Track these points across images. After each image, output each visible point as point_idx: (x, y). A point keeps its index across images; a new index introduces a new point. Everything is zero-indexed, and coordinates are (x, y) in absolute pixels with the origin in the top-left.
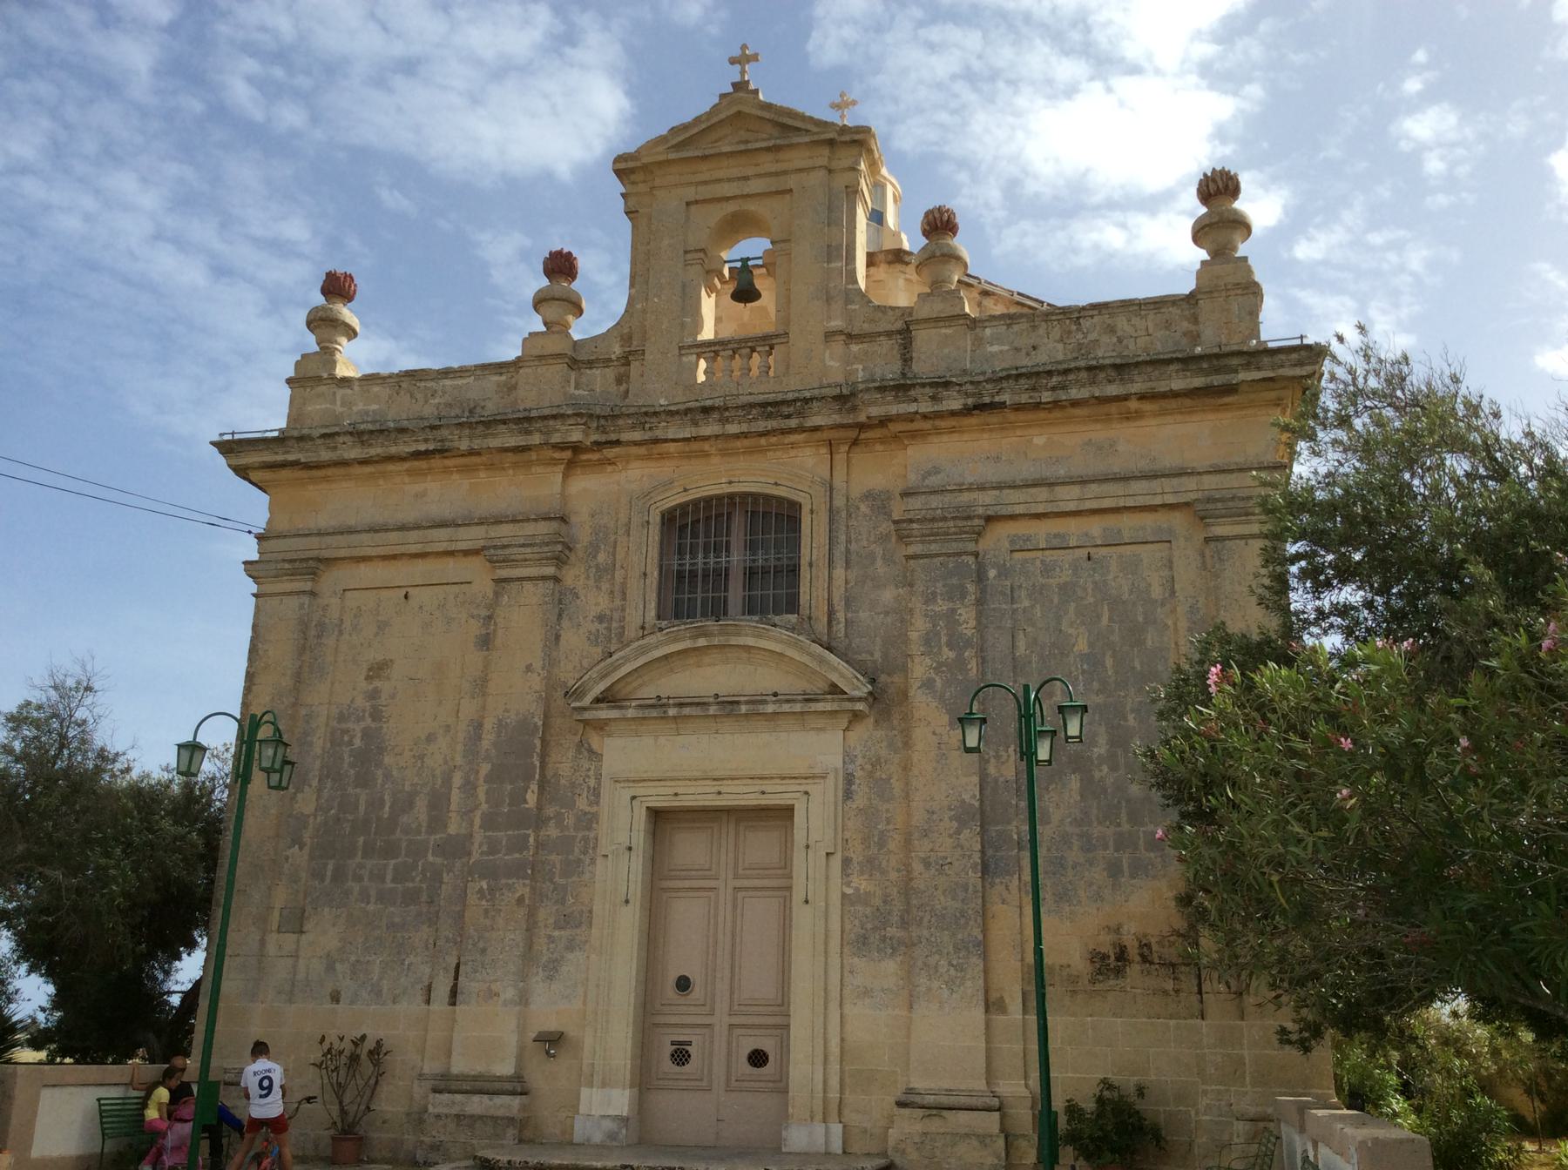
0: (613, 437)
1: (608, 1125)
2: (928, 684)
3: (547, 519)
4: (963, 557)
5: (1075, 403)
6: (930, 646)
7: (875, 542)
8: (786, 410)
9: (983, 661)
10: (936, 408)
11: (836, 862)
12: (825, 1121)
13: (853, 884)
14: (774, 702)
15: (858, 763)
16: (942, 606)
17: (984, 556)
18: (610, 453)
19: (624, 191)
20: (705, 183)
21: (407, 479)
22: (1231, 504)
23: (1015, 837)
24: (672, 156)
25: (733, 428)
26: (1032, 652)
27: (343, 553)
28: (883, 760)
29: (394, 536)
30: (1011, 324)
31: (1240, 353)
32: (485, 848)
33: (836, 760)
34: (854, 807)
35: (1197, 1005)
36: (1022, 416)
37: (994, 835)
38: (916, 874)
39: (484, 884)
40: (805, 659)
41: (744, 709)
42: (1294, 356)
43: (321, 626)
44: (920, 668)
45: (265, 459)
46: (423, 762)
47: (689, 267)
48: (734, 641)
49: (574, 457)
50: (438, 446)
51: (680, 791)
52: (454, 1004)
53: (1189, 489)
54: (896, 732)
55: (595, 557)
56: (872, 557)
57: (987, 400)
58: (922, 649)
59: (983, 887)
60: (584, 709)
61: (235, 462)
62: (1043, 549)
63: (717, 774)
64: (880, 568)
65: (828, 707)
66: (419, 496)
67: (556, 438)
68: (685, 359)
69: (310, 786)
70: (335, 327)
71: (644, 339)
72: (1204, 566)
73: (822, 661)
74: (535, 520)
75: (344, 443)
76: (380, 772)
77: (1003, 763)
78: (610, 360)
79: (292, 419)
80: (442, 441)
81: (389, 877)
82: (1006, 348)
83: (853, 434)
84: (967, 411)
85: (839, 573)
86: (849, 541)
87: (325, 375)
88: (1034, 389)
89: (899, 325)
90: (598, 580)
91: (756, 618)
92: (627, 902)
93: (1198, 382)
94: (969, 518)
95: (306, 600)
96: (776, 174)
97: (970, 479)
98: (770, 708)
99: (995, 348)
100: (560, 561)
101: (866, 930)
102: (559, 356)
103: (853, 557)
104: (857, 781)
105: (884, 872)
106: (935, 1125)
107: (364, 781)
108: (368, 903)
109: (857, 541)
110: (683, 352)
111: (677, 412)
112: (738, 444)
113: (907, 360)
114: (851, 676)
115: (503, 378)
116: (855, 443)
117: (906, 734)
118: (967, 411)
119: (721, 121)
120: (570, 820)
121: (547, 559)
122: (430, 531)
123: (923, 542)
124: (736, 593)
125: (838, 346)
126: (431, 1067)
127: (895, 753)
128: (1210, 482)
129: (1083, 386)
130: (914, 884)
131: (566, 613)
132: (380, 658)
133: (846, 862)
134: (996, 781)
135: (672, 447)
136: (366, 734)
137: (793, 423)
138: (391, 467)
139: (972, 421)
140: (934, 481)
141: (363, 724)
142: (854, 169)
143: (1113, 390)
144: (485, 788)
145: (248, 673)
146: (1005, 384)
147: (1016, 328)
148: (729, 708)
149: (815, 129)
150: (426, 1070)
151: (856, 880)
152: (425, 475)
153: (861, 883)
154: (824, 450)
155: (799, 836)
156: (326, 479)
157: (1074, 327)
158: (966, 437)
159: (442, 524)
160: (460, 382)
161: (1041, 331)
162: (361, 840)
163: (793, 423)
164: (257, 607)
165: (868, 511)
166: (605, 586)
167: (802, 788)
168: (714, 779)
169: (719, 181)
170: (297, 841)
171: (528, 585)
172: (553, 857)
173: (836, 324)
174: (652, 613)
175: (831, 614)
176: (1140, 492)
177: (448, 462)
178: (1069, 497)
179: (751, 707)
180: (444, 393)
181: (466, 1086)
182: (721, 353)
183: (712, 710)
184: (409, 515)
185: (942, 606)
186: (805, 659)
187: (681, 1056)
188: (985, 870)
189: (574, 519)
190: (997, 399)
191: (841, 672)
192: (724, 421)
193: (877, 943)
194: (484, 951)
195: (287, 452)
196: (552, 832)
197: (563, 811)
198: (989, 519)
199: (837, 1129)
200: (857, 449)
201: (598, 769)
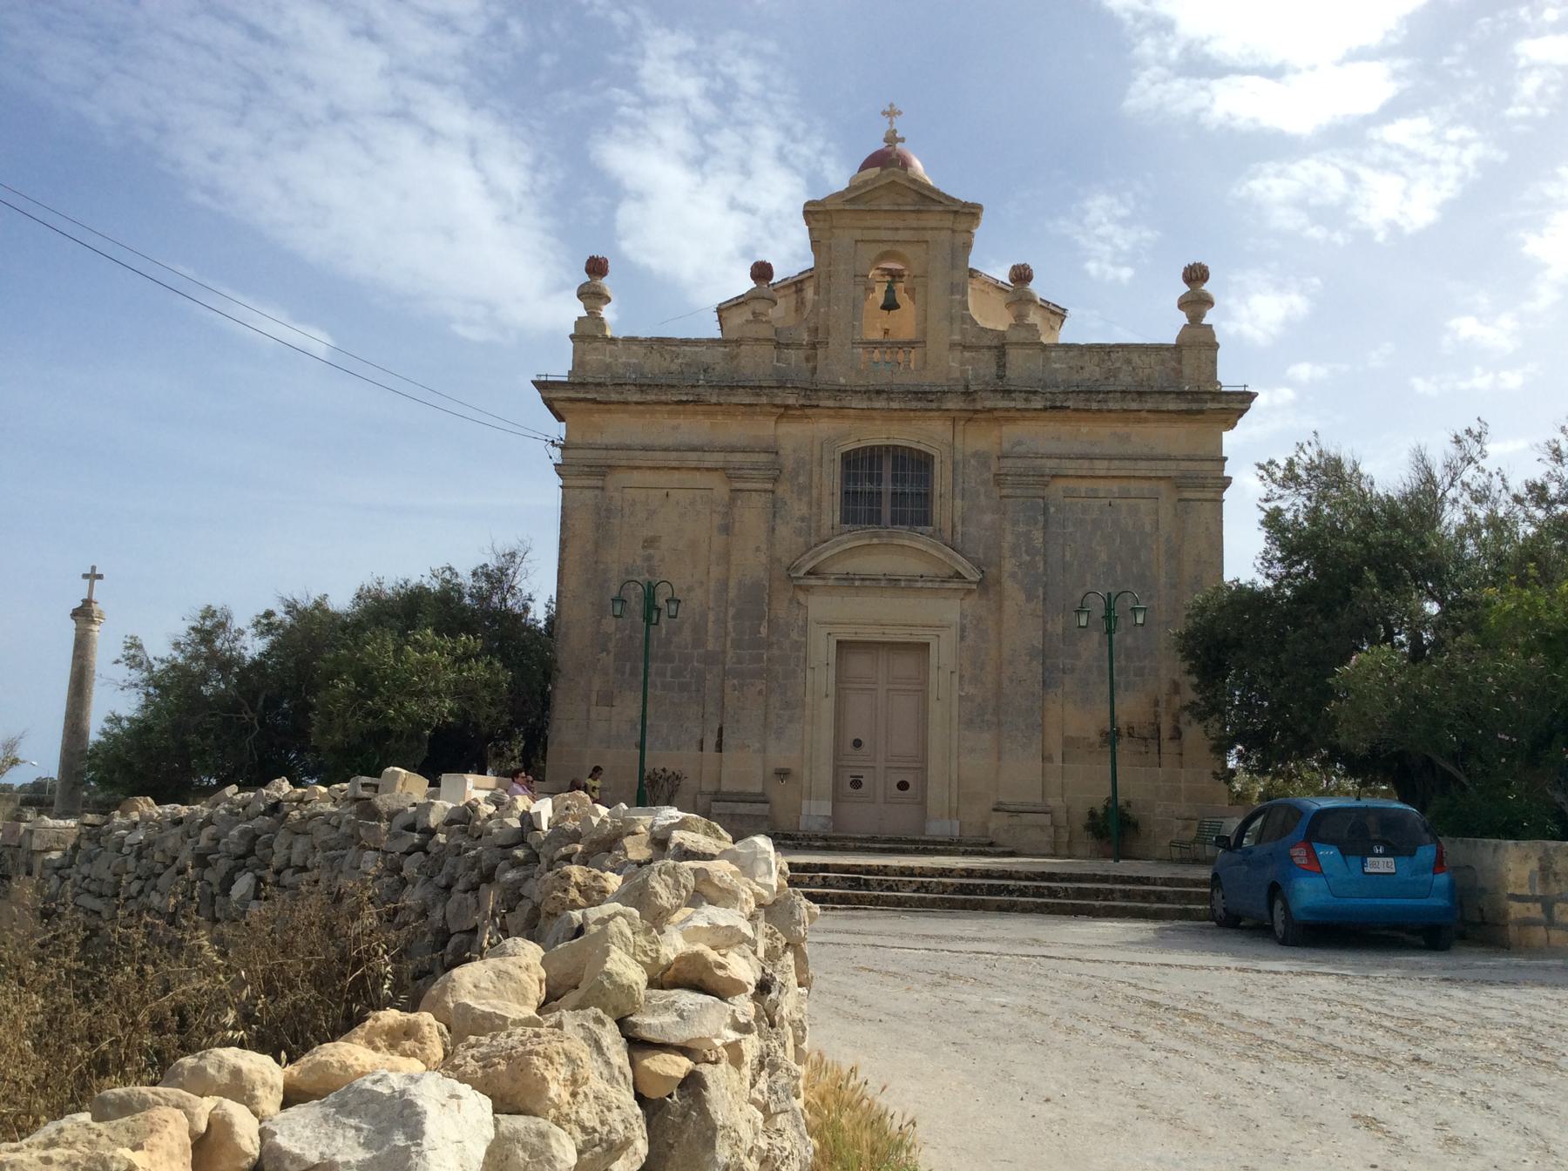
0: (815, 403)
1: (822, 821)
2: (1013, 575)
5: (1110, 411)
8: (931, 397)
9: (1045, 562)
11: (956, 678)
12: (950, 818)
16: (1022, 528)
18: (809, 412)
20: (869, 228)
21: (666, 416)
22: (1196, 481)
24: (847, 207)
25: (894, 405)
27: (624, 463)
29: (658, 455)
31: (1210, 393)
32: (734, 660)
35: (1157, 759)
36: (1078, 415)
38: (1004, 686)
39: (735, 682)
41: (903, 584)
42: (1240, 397)
43: (608, 510)
44: (1009, 565)
48: (896, 541)
49: (784, 412)
50: (696, 398)
52: (721, 751)
53: (1171, 468)
57: (1058, 404)
60: (800, 578)
61: (547, 395)
63: (883, 622)
64: (983, 500)
65: (955, 586)
66: (676, 428)
67: (778, 401)
68: (855, 351)
71: (828, 333)
72: (1176, 515)
73: (951, 557)
74: (759, 452)
78: (802, 345)
79: (578, 363)
82: (1064, 366)
83: (970, 415)
84: (1045, 409)
85: (958, 502)
87: (600, 336)
88: (1087, 400)
89: (995, 342)
91: (907, 527)
93: (1184, 406)
94: (1042, 476)
97: (1042, 451)
98: (919, 585)
99: (1057, 366)
100: (775, 480)
102: (770, 340)
106: (1015, 820)
111: (860, 392)
112: (896, 414)
113: (1002, 366)
115: (727, 350)
116: (970, 420)
117: (1000, 608)
118: (1045, 409)
124: (886, 511)
125: (957, 353)
126: (708, 787)
128: (1184, 465)
129: (1117, 402)
133: (961, 677)
135: (852, 412)
138: (658, 408)
139: (1046, 414)
140: (1021, 449)
143: (1134, 406)
146: (1070, 396)
147: (1071, 354)
148: (893, 583)
149: (946, 202)
150: (704, 789)
153: (970, 689)
154: (949, 423)
155: (933, 660)
156: (609, 411)
157: (1106, 358)
158: (1040, 423)
159: (694, 449)
160: (697, 349)
161: (1087, 358)
163: (934, 405)
164: (563, 495)
165: (976, 464)
166: (805, 499)
170: (605, 649)
173: (957, 338)
174: (837, 519)
175: (953, 527)
176: (1143, 468)
177: (697, 408)
178: (1101, 467)
180: (685, 356)
181: (735, 798)
183: (883, 583)
184: (668, 439)
185: (1022, 528)
186: (941, 556)
187: (856, 783)
188: (1045, 684)
189: (781, 452)
190: (1065, 404)
191: (964, 567)
192: (890, 399)
196: (776, 652)
198: (1054, 476)
199: (957, 823)
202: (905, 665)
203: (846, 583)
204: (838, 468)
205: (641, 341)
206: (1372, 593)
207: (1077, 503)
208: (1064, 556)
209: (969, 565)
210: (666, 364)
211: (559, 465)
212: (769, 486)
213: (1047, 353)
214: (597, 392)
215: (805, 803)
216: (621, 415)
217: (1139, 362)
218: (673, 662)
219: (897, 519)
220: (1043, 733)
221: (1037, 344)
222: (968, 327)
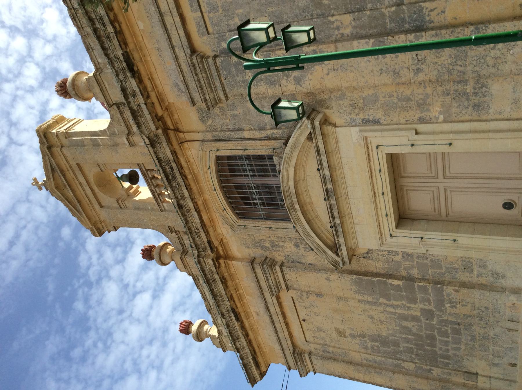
0: (207, 245)
3: (254, 269)
4: (218, 66)
6: (274, 81)
7: (226, 115)
8: (168, 170)
10: (139, 93)
11: (421, 127)
13: (437, 116)
14: (323, 171)
15: (355, 118)
17: (215, 51)
18: (216, 243)
19: (107, 232)
21: (252, 318)
23: (393, 9)
25: (186, 194)
26: (266, 12)
27: (289, 342)
28: (351, 103)
30: (92, 48)
33: (355, 131)
34: (383, 118)
36: (129, 40)
37: (393, 25)
38: (426, 78)
39: (448, 306)
40: (295, 154)
41: (330, 186)
45: (255, 369)
46: (384, 321)
47: (127, 206)
48: (293, 191)
51: (384, 214)
54: (332, 96)
55: (268, 247)
56: (234, 116)
57: (124, 64)
58: (277, 86)
59: (432, 29)
60: (343, 261)
62: (202, 13)
63: (371, 195)
66: (258, 314)
67: (214, 269)
68: (167, 208)
69: (401, 364)
70: (200, 332)
73: (295, 146)
75: (240, 345)
76: (391, 338)
77: (342, 23)
80: (228, 311)
81: (446, 339)
83: (171, 133)
85: (246, 134)
86: (229, 130)
88: (108, 37)
90: (278, 246)
92: (455, 241)
95: (313, 357)
96: (73, 171)
98: (327, 173)
100: (272, 263)
101: (469, 105)
103: (237, 127)
104: (367, 117)
105: (427, 96)
107: (396, 344)
108: (461, 348)
109: (227, 125)
110: (163, 209)
114: (299, 131)
116: (177, 130)
119: (62, 195)
120: (408, 264)
121: (272, 270)
122: (271, 312)
123: (216, 91)
127: (346, 95)
130: (434, 78)
131: (298, 260)
132: (334, 332)
133: (422, 121)
134: (355, 27)
135: (205, 218)
136: (373, 341)
137: (174, 165)
140: (182, 86)
141: (368, 341)
142: (57, 135)
144: (393, 301)
145: (350, 379)
146: (112, 56)
149: (47, 158)
151: (434, 114)
152: (247, 312)
153: (436, 110)
154: (186, 145)
158: (153, 70)
159: (268, 308)
162: (427, 348)
163: (174, 165)
164: (320, 373)
167: (374, 149)
168: (375, 196)
169: (86, 195)
171: (287, 277)
172: (430, 272)
175: (268, 138)
177: (238, 305)
179: (328, 182)
182: (158, 192)
183: (333, 202)
186: (295, 154)
190: (122, 59)
192: (183, 198)
193: (478, 98)
194: (487, 308)
195: (250, 362)
197: (403, 266)
200: (181, 128)
201: (377, 250)
204: (249, 223)
205: (214, 320)
207: (210, 18)
214: (247, 358)
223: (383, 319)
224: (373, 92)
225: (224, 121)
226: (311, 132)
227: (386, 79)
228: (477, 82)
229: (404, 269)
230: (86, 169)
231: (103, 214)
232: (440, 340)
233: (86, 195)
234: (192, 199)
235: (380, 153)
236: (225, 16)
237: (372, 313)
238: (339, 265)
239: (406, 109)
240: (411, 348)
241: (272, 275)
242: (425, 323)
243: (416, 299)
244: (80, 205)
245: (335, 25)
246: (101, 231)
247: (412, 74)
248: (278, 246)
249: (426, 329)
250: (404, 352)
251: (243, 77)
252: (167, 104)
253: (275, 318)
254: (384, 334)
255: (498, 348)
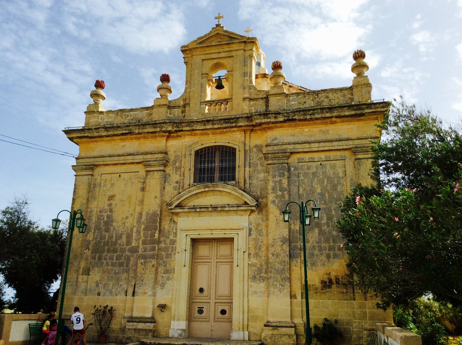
0: (181, 129)
1: (180, 332)
2: (273, 202)
3: (161, 153)
7: (258, 160)
10: (276, 120)
11: (246, 254)
14: (228, 207)
16: (277, 179)
18: (180, 134)
19: (184, 56)
20: (208, 54)
22: (363, 149)
23: (299, 247)
24: (198, 46)
25: (216, 126)
27: (101, 163)
29: (116, 158)
31: (365, 104)
32: (143, 250)
34: (252, 238)
36: (301, 123)
38: (270, 258)
39: (143, 261)
40: (237, 194)
41: (219, 209)
42: (381, 105)
43: (95, 184)
44: (271, 197)
46: (125, 225)
48: (216, 189)
49: (169, 135)
53: (350, 144)
54: (264, 216)
55: (175, 164)
57: (291, 118)
58: (272, 191)
59: (290, 261)
60: (172, 209)
61: (69, 136)
63: (211, 228)
64: (260, 168)
65: (244, 208)
67: (164, 129)
68: (202, 106)
71: (190, 100)
72: (355, 167)
73: (242, 195)
74: (158, 153)
78: (180, 106)
82: (296, 103)
83: (251, 128)
84: (285, 121)
85: (247, 169)
86: (250, 160)
88: (305, 115)
89: (265, 96)
90: (176, 171)
91: (223, 182)
92: (185, 266)
93: (353, 113)
94: (286, 153)
96: (229, 51)
98: (227, 209)
99: (293, 103)
100: (165, 165)
103: (251, 164)
104: (253, 230)
105: (260, 257)
106: (275, 332)
107: (107, 230)
109: (253, 159)
112: (218, 131)
113: (267, 106)
115: (148, 111)
116: (252, 130)
117: (267, 217)
118: (285, 121)
119: (212, 36)
120: (168, 242)
121: (161, 165)
123: (272, 160)
124: (217, 175)
125: (247, 102)
126: (127, 315)
129: (319, 114)
130: (269, 261)
132: (112, 194)
133: (249, 254)
134: (293, 230)
135: (198, 132)
136: (108, 217)
137: (234, 125)
138: (115, 138)
140: (275, 142)
141: (107, 214)
143: (328, 115)
145: (73, 198)
146: (296, 113)
147: (299, 97)
148: (215, 208)
150: (126, 316)
153: (254, 260)
154: (243, 133)
156: (96, 141)
158: (285, 129)
159: (130, 155)
161: (307, 98)
162: (106, 248)
163: (234, 125)
164: (76, 179)
165: (256, 151)
166: (178, 173)
169: (212, 53)
171: (155, 173)
172: (163, 253)
173: (247, 95)
175: (245, 181)
176: (336, 145)
178: (315, 147)
179: (221, 208)
181: (137, 320)
182: (213, 104)
183: (210, 209)
184: (121, 152)
185: (277, 179)
186: (237, 194)
187: (201, 311)
189: (169, 153)
190: (294, 118)
191: (248, 199)
192: (213, 124)
194: (142, 280)
195: (85, 133)
196: (163, 245)
199: (246, 333)
200: (253, 133)
201: (176, 227)
202: (224, 249)
203: (193, 210)
204: (193, 157)
205: (113, 112)
206: (438, 179)
208: (299, 191)
209: (250, 198)
210: (123, 120)
211: (74, 166)
212: (162, 168)
213: (288, 97)
214: (89, 133)
215: (172, 322)
216: (101, 143)
217: (332, 97)
218: (117, 253)
219: (222, 179)
220: (290, 283)
221: (282, 93)
222: (253, 90)
223: (126, 225)
224: (264, 234)
225: (255, 158)
226: (249, 204)
227: (271, 241)
228: (265, 278)
229: (165, 240)
230: (228, 60)
231: (198, 59)
232: (114, 255)
233: (212, 53)
234: (211, 129)
235: (234, 234)
236: (305, 173)
237: (130, 219)
238: (169, 207)
239: (255, 248)
240: (105, 238)
241: (158, 164)
242: (126, 248)
243: (146, 244)
244: (206, 46)
245: (295, 222)
246: (184, 51)
247: (272, 252)
248: (176, 171)
249: (121, 248)
250: (101, 235)
251: (277, 175)
252: (267, 130)
253: (122, 158)
254: (114, 224)
255: (111, 286)
